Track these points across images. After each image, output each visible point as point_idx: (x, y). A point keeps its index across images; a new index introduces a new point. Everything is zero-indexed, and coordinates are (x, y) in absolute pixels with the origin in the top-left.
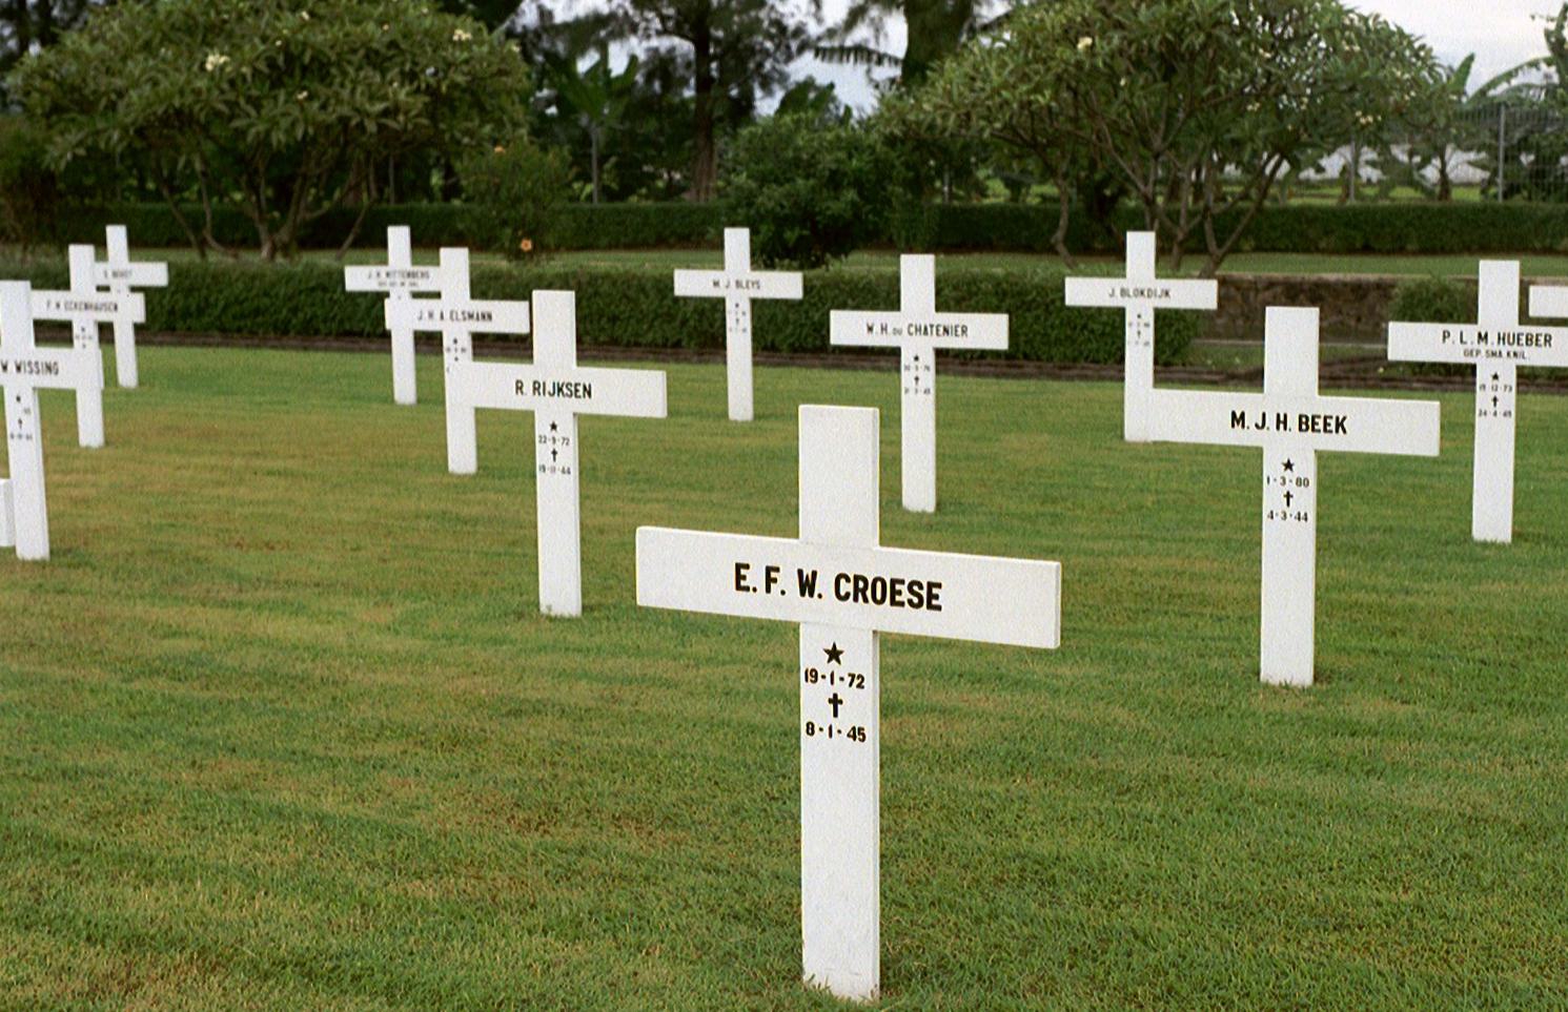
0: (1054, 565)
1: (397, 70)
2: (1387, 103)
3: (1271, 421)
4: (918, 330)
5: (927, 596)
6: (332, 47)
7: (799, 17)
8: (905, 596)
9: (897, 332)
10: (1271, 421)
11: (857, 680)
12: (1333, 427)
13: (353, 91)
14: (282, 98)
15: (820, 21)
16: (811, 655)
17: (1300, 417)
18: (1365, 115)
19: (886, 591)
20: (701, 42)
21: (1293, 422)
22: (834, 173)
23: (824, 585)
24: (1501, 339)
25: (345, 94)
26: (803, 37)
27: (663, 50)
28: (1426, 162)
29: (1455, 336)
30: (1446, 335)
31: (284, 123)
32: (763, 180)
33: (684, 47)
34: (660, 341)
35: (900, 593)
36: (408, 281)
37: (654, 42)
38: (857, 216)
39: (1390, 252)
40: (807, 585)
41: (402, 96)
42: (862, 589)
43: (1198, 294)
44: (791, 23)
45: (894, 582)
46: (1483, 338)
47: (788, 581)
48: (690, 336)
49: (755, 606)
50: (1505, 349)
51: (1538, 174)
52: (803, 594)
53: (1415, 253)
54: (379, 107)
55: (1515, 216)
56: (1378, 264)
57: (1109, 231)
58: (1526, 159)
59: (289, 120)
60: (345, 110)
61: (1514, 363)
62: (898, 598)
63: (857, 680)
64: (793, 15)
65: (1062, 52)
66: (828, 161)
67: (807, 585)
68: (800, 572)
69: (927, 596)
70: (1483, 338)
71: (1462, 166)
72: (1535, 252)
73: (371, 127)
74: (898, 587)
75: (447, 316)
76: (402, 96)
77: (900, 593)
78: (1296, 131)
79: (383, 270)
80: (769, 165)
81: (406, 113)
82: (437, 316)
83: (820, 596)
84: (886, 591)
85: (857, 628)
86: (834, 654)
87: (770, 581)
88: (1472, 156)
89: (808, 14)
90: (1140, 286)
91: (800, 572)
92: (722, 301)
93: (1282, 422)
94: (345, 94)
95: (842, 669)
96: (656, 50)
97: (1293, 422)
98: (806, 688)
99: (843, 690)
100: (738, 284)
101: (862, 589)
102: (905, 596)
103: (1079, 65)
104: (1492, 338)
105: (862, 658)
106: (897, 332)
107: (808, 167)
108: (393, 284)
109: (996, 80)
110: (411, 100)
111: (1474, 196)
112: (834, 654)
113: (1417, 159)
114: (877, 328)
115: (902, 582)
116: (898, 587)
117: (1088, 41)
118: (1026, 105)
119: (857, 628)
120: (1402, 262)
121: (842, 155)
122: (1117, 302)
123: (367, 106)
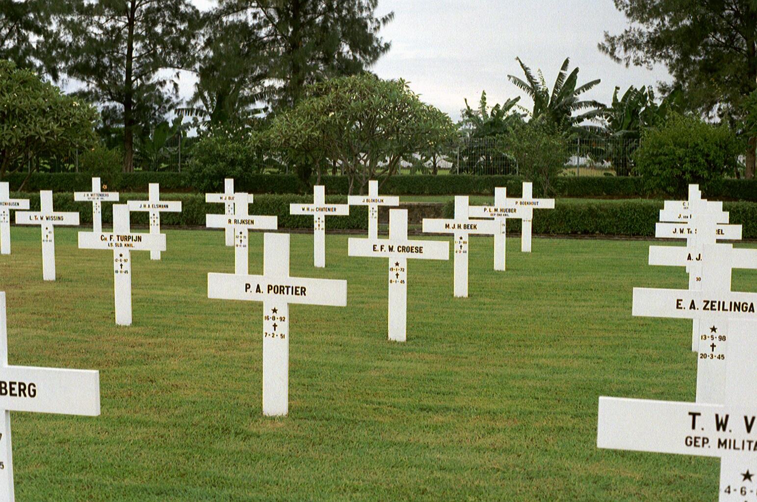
0: (95, 372)
1: (51, 117)
2: (438, 137)
3: (456, 226)
4: (319, 209)
5: (419, 250)
6: (26, 108)
7: (169, 94)
8: (414, 250)
9: (312, 210)
10: (456, 226)
11: (403, 270)
12: (300, 292)
13: (35, 125)
14: (5, 128)
15: (177, 97)
16: (391, 264)
17: (269, 286)
18: (431, 141)
19: (409, 249)
20: (128, 105)
21: (462, 227)
22: (232, 160)
23: (395, 249)
24: (501, 210)
25: (32, 126)
26: (171, 103)
27: (110, 108)
28: (428, 158)
29: (488, 210)
30: (485, 210)
31: (8, 138)
32: (205, 163)
33: (120, 106)
34: (171, 223)
35: (14, 389)
36: (100, 197)
37: (107, 104)
38: (241, 176)
39: (418, 194)
40: (391, 249)
41: (55, 127)
42: (404, 249)
43: (175, 207)
44: (166, 97)
45: (11, 383)
46: (496, 210)
47: (386, 248)
48: (183, 220)
49: (378, 254)
50: (503, 213)
51: (470, 164)
52: (718, 429)
53: (428, 195)
54: (46, 132)
55: (467, 181)
56: (427, 196)
57: (308, 185)
58: (465, 159)
59: (10, 136)
60: (33, 133)
61: (505, 218)
62: (13, 392)
63: (403, 270)
64: (166, 93)
65: (323, 118)
66: (230, 156)
67: (391, 249)
68: (717, 416)
69: (419, 250)
70: (496, 210)
71: (443, 162)
72: (474, 194)
73: (43, 140)
74: (13, 386)
75: (151, 206)
76: (55, 127)
77: (14, 389)
78: (406, 146)
79: (90, 193)
80: (205, 157)
81: (57, 135)
82: (147, 206)
83: (730, 431)
84: (409, 249)
85: (402, 258)
86: (275, 311)
87: (382, 249)
88: (445, 157)
89: (173, 93)
90: (373, 198)
91: (717, 416)
92: (148, 213)
93: (459, 227)
94: (32, 126)
95: (399, 267)
96: (108, 107)
97: (462, 227)
98: (265, 322)
99: (277, 322)
100: (229, 198)
101: (404, 249)
102: (414, 250)
103: (328, 122)
104: (499, 210)
105: (404, 264)
106: (312, 210)
107: (222, 158)
108: (94, 199)
109: (299, 127)
110: (59, 129)
111: (447, 173)
112: (397, 264)
113: (424, 158)
114: (306, 209)
115: (15, 383)
116: (13, 386)
117: (333, 113)
118: (310, 136)
119: (402, 258)
120: (423, 198)
121: (235, 153)
122: (365, 204)
123: (41, 131)
